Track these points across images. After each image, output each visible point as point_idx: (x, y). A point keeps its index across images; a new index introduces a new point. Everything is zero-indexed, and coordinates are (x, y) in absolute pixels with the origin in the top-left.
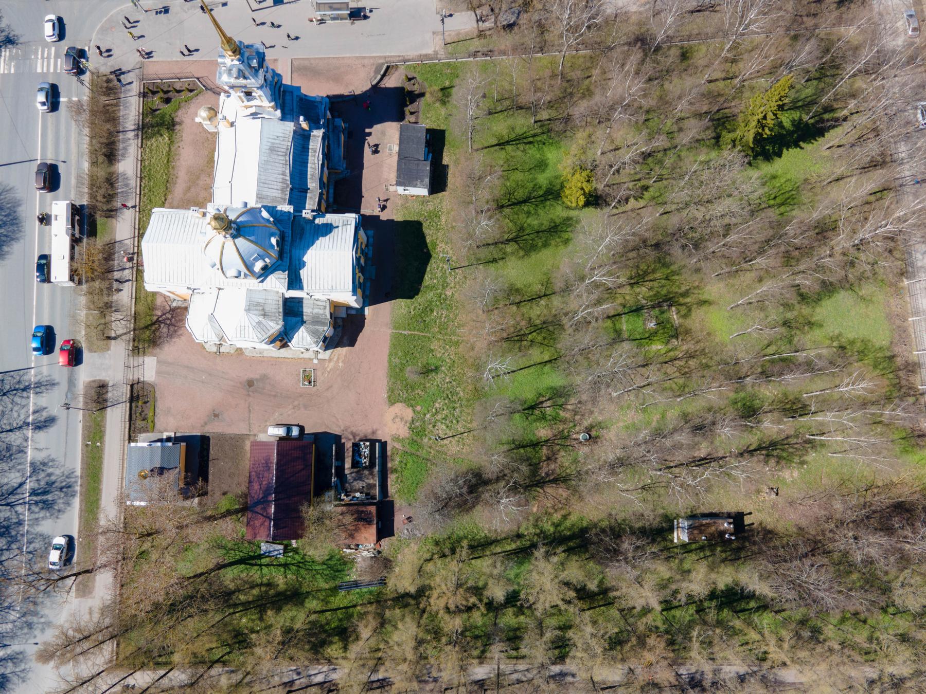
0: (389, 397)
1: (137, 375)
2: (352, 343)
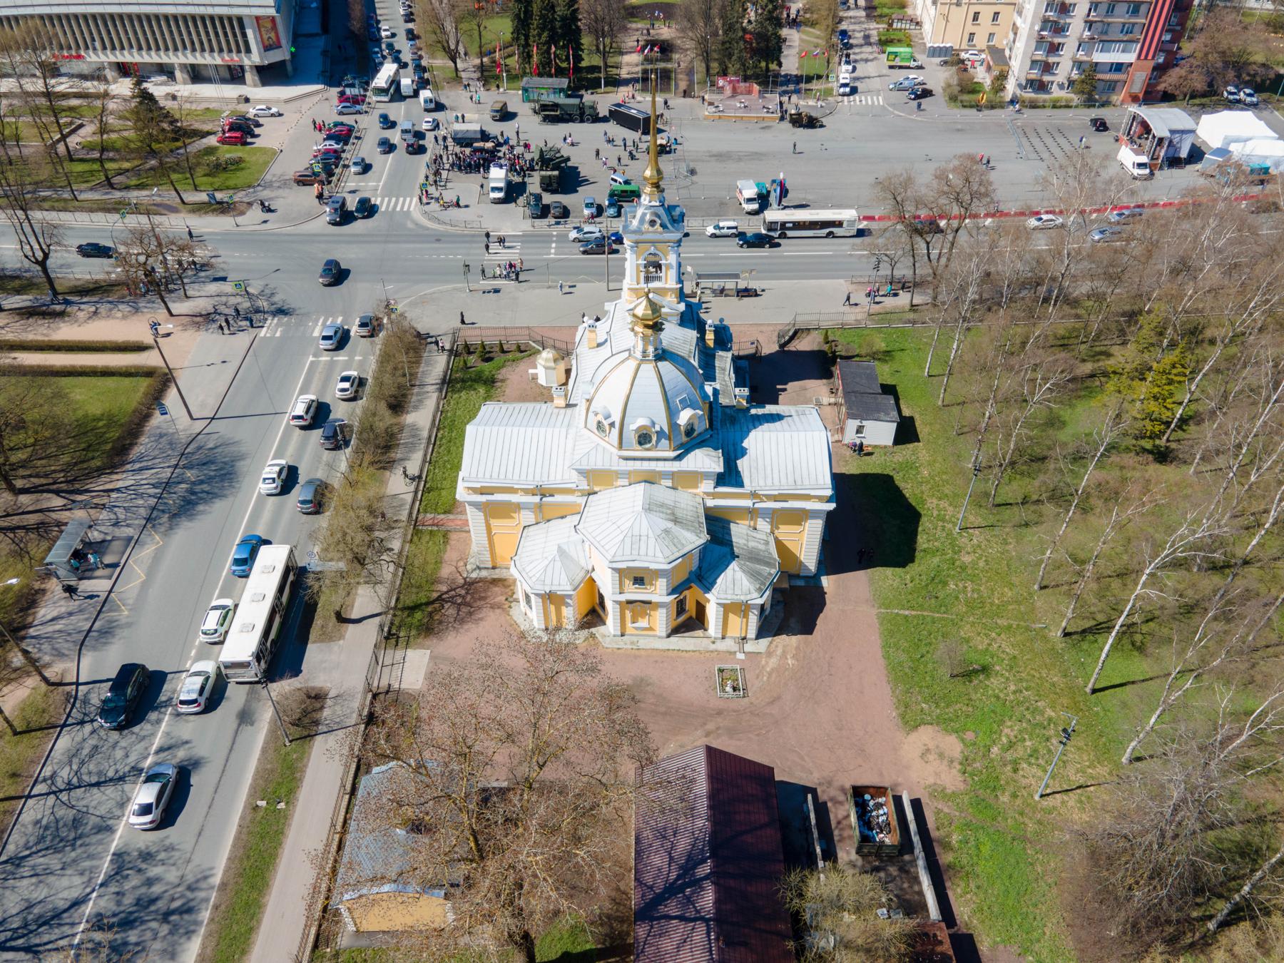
0: (903, 716)
1: (384, 680)
2: (807, 627)
